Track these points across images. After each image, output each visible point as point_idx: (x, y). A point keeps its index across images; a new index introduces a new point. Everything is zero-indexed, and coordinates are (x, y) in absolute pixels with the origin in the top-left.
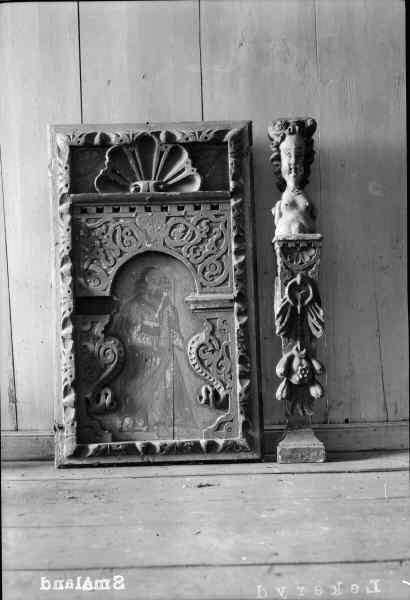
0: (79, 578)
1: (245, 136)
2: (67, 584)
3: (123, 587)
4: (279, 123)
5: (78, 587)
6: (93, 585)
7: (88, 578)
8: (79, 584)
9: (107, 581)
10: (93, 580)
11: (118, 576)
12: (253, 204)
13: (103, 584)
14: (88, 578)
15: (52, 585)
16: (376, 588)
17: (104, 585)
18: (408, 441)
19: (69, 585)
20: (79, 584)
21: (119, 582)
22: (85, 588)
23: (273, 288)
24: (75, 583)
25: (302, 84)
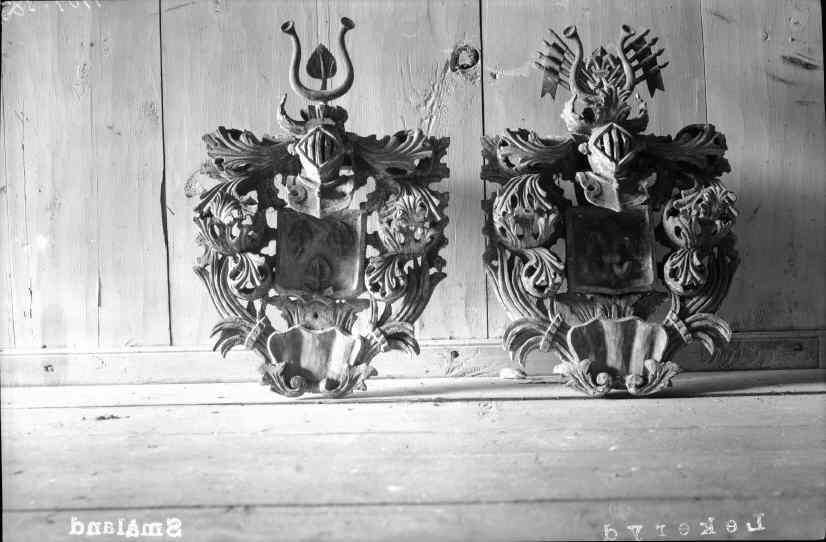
0: (121, 523)
1: (725, 167)
2: (106, 527)
3: (179, 534)
4: (209, 269)
5: (120, 533)
6: (141, 530)
7: (133, 522)
8: (120, 529)
9: (159, 525)
10: (140, 523)
11: (174, 535)
12: (403, 401)
13: (153, 529)
14: (133, 522)
15: (86, 529)
16: (760, 525)
17: (155, 531)
18: (821, 58)
19: (108, 528)
20: (120, 529)
21: (174, 526)
22: (129, 534)
23: (578, 353)
24: (116, 527)
25: (322, 64)
